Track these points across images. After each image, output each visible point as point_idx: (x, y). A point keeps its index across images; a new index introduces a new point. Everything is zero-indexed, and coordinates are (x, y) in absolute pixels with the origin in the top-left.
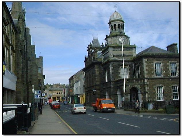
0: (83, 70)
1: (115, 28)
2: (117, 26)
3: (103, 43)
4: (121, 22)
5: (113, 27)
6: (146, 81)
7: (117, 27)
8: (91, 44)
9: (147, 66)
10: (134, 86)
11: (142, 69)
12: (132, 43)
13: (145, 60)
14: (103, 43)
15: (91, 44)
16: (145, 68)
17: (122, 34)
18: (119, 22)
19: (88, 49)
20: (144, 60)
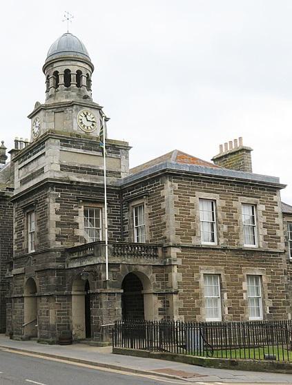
1: (67, 83)
2: (73, 77)
4: (87, 66)
5: (62, 80)
6: (174, 252)
7: (68, 74)
11: (43, 221)
12: (114, 133)
16: (54, 217)
17: (86, 103)
18: (79, 64)
20: (169, 189)
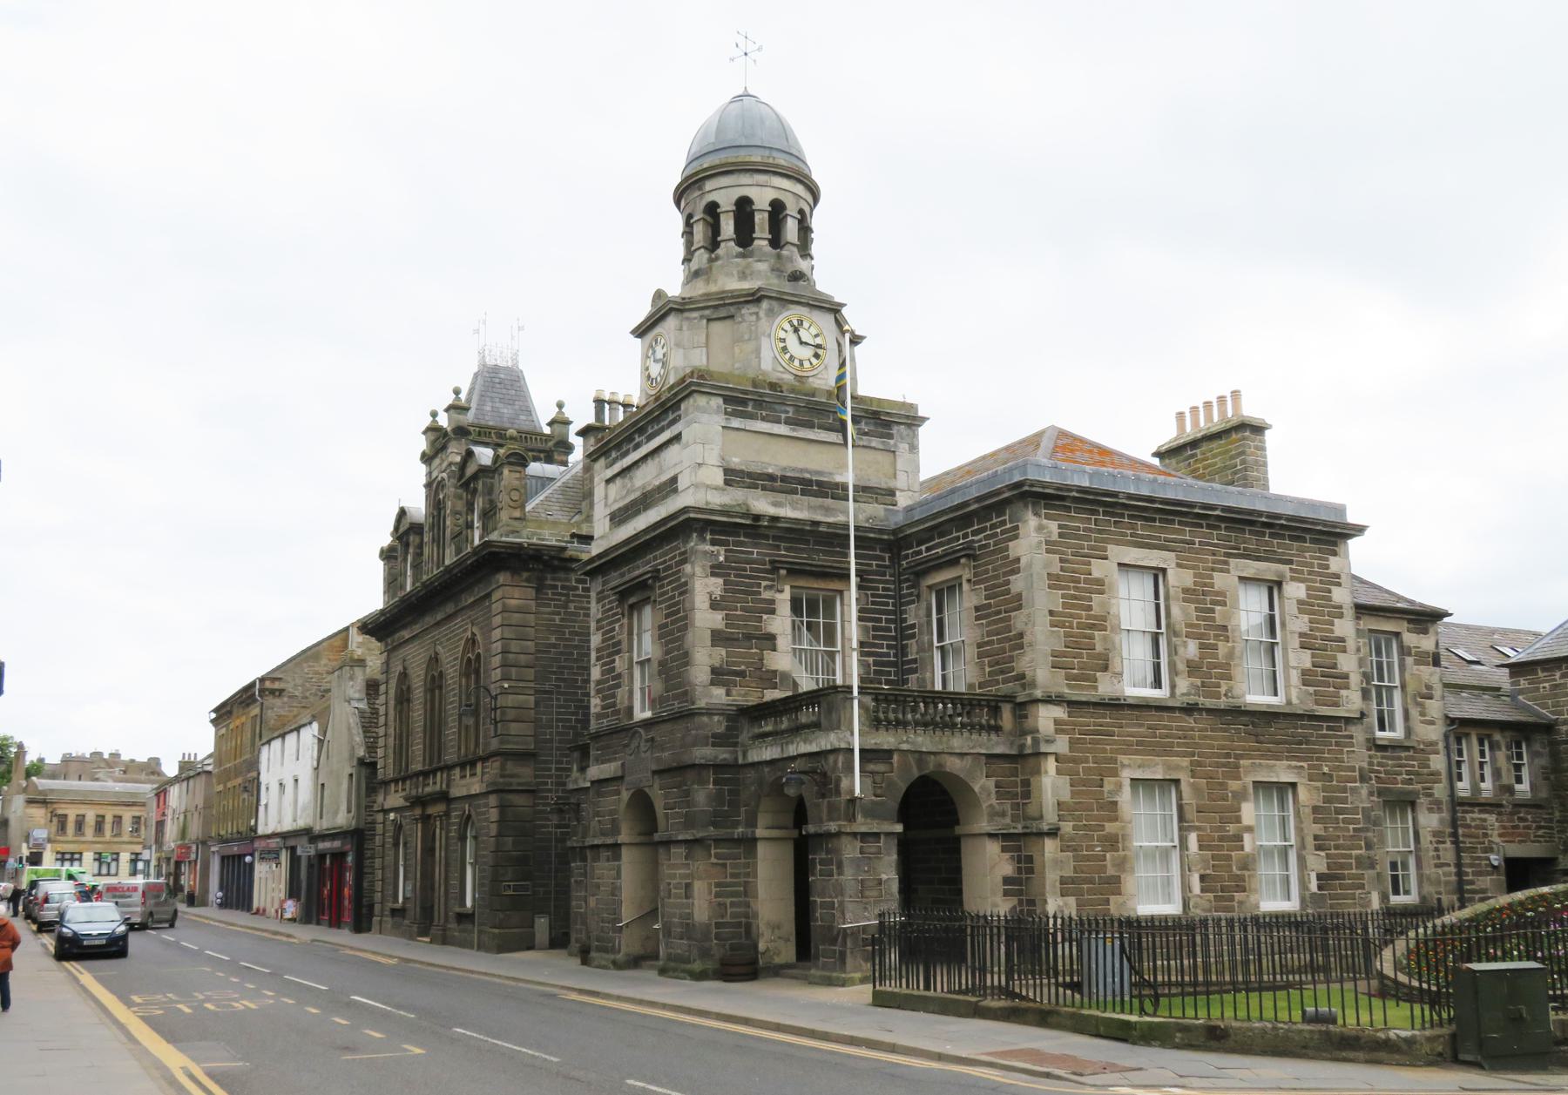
0: (376, 627)
1: (744, 236)
2: (761, 220)
3: (560, 405)
4: (799, 189)
5: (728, 227)
6: (1046, 718)
8: (463, 396)
9: (1055, 581)
10: (931, 766)
11: (674, 631)
13: (1040, 528)
14: (560, 405)
15: (463, 396)
16: (706, 619)
19: (432, 443)
